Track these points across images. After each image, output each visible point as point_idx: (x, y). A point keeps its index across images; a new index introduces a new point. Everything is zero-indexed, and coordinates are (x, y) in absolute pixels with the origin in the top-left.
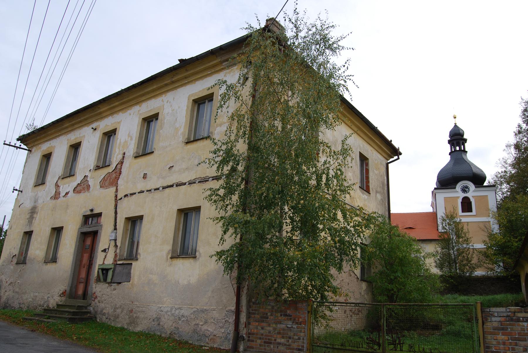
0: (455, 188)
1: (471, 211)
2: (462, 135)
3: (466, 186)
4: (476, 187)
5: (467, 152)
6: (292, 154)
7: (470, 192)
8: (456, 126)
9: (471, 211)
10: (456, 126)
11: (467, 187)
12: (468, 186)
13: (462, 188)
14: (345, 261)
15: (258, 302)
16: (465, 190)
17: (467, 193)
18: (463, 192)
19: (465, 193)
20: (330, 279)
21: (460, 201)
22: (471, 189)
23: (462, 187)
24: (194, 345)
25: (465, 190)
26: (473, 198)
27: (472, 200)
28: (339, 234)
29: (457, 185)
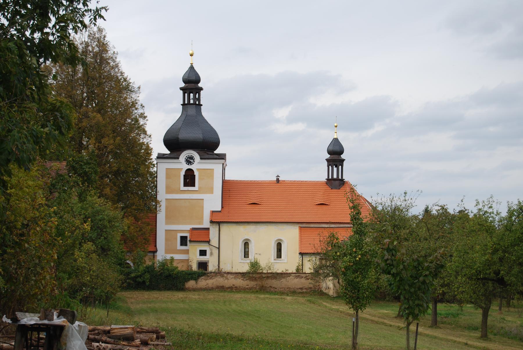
0: (178, 158)
1: (194, 185)
2: (198, 81)
3: (191, 156)
4: (201, 159)
5: (202, 105)
6: (50, 19)
7: (195, 163)
8: (192, 68)
9: (194, 185)
10: (192, 68)
11: (192, 158)
12: (193, 157)
13: (186, 158)
14: (113, 186)
15: (10, 195)
16: (189, 160)
17: (191, 165)
18: (186, 163)
19: (188, 164)
20: (306, 298)
21: (183, 173)
22: (196, 160)
23: (187, 157)
24: (117, 208)
25: (189, 160)
26: (198, 171)
27: (196, 173)
28: (93, 99)
29: (183, 153)
